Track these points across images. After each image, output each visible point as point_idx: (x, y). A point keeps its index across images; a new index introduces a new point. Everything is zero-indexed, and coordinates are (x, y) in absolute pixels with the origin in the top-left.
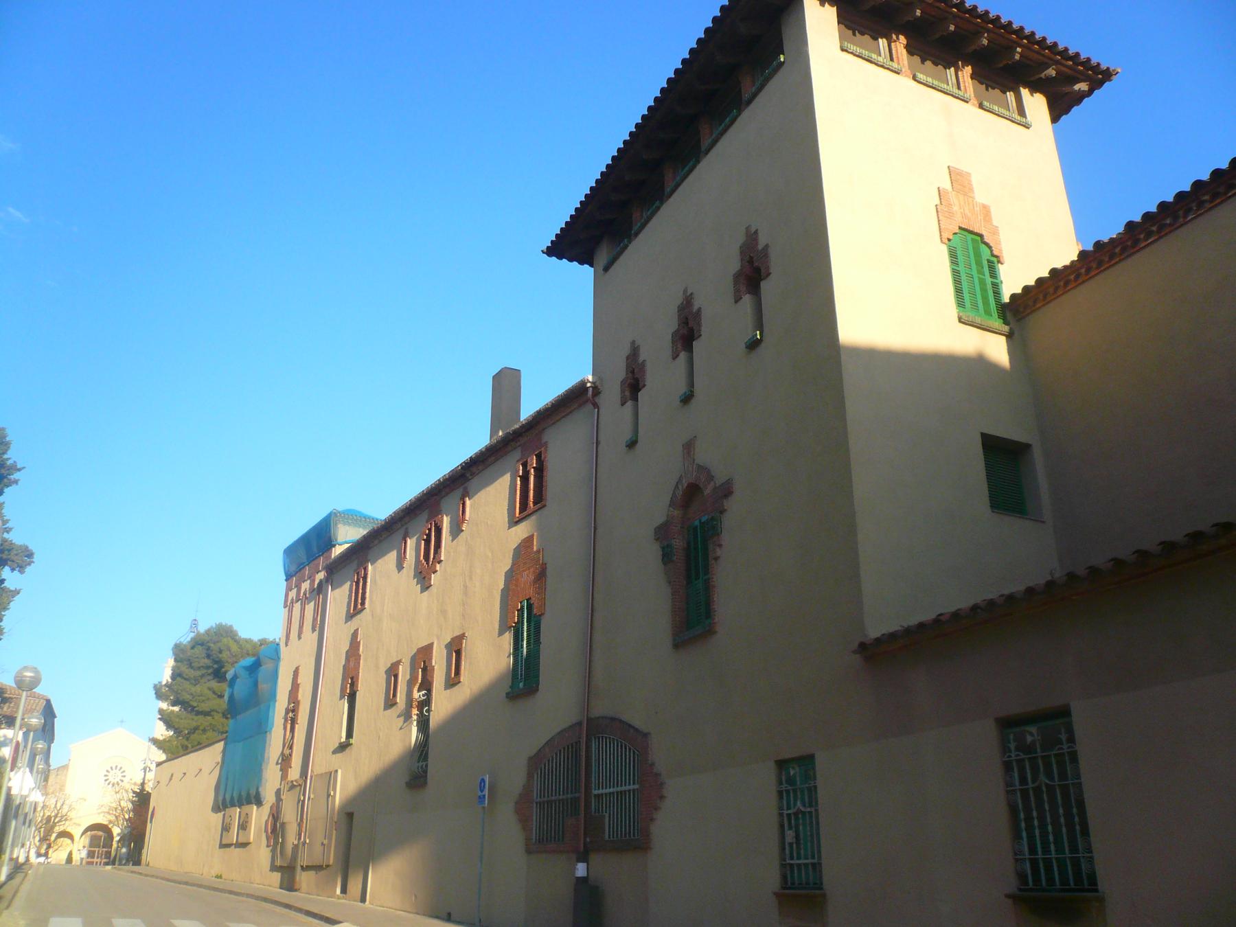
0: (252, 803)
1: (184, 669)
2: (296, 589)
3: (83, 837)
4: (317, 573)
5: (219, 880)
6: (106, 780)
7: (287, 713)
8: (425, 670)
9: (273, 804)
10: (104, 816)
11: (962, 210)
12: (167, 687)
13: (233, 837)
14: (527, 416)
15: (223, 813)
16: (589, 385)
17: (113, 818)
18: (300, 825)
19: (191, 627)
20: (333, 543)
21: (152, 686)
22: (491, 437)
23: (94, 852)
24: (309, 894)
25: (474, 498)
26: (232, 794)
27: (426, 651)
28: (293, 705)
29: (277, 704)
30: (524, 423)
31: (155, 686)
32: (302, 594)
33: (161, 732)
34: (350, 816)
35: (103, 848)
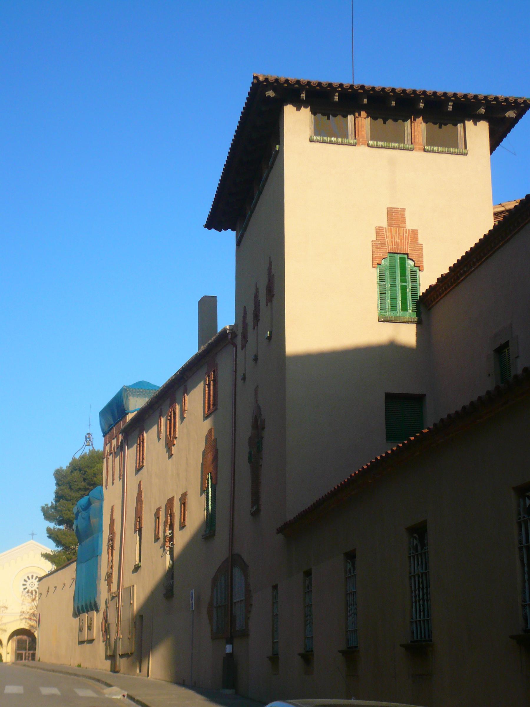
0: (93, 610)
1: (67, 491)
2: (109, 444)
3: (11, 641)
4: (113, 439)
5: (79, 668)
6: (25, 589)
7: (109, 542)
8: (171, 514)
9: (105, 610)
10: (26, 622)
11: (393, 240)
12: (53, 508)
13: (85, 636)
14: (221, 329)
15: (79, 617)
16: (228, 331)
17: (33, 623)
18: (117, 625)
19: (86, 440)
20: (126, 412)
21: (40, 509)
22: (199, 350)
23: (22, 654)
24: (124, 674)
25: (189, 395)
26: (82, 603)
27: (170, 501)
28: (111, 535)
29: (103, 534)
30: (203, 349)
31: (43, 509)
32: (112, 450)
33: (51, 547)
34: (141, 617)
35: (29, 650)
